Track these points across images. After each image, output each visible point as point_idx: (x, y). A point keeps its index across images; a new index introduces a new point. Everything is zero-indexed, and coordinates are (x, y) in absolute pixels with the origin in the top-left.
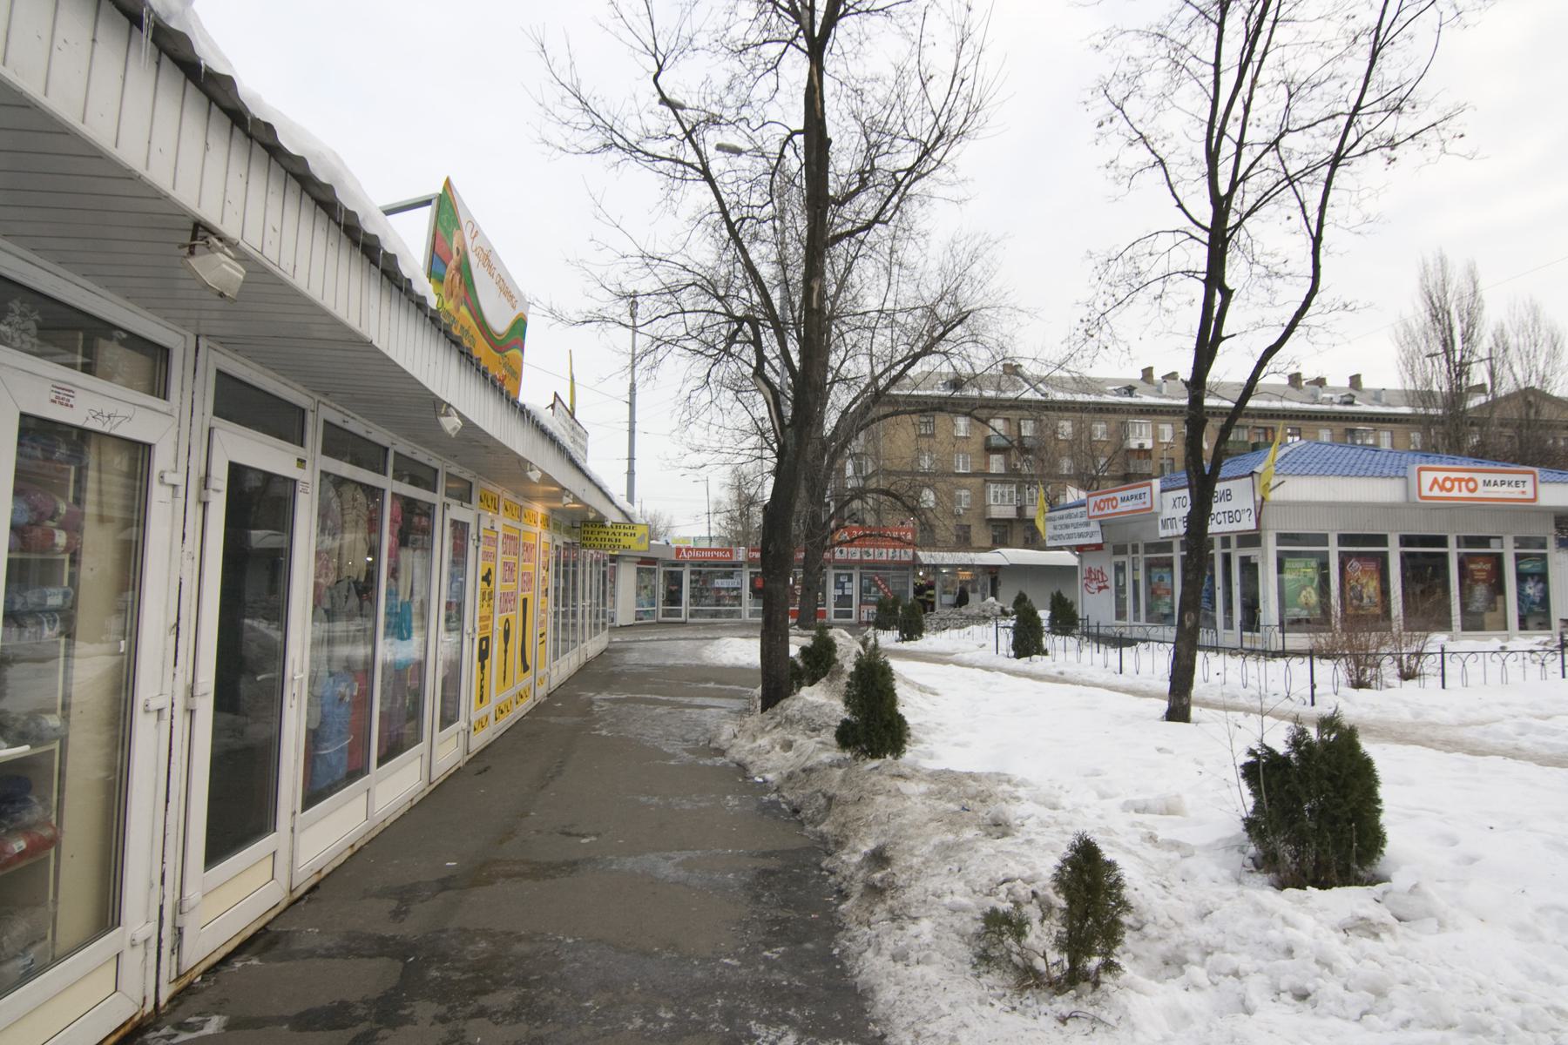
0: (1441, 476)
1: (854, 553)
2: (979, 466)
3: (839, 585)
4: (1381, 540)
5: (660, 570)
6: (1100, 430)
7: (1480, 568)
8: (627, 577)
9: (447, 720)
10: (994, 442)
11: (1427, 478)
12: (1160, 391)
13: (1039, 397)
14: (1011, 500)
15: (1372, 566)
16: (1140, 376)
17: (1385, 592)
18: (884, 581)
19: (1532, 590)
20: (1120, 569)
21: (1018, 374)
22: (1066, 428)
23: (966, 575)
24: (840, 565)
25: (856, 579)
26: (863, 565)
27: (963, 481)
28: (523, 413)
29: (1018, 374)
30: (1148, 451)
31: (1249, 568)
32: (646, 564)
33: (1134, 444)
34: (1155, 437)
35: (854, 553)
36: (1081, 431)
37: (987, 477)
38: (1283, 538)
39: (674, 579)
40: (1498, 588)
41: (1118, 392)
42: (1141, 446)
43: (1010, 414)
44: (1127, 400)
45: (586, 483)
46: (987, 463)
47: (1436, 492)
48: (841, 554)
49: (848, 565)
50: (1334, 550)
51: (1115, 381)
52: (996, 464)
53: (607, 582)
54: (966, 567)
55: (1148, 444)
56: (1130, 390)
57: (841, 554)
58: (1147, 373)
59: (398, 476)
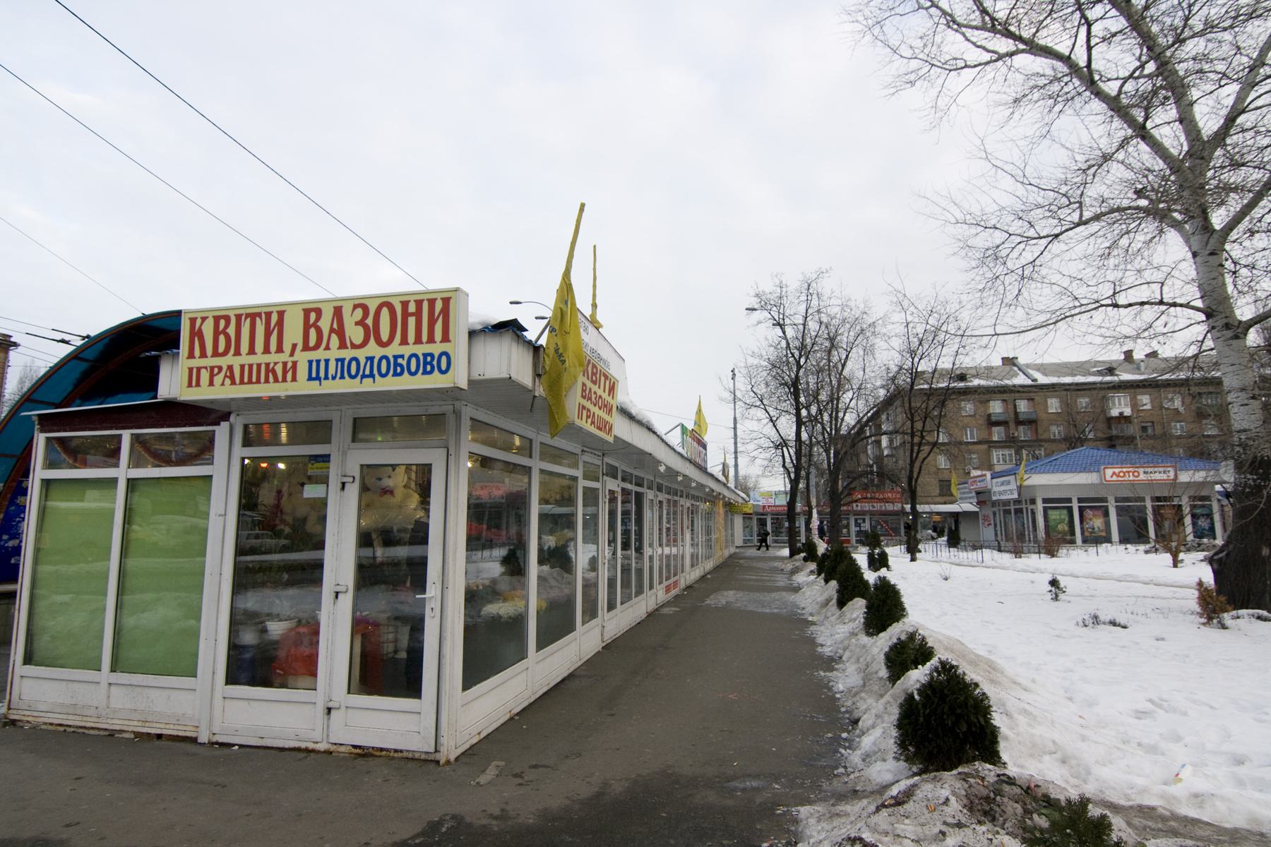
0: (1117, 471)
1: (867, 506)
2: (984, 435)
3: (857, 525)
4: (1069, 500)
5: (755, 518)
6: (1083, 401)
7: (1168, 513)
8: (738, 521)
9: (661, 583)
10: (993, 419)
11: (1109, 472)
12: (1138, 368)
13: (1029, 382)
14: (1011, 460)
15: (1100, 513)
16: (1122, 357)
17: (1108, 524)
18: (886, 522)
19: (1203, 523)
20: (994, 514)
21: (1014, 365)
22: (1054, 405)
23: (937, 518)
24: (856, 513)
25: (868, 521)
26: (872, 513)
27: (970, 447)
28: (712, 476)
29: (1014, 365)
30: (1126, 417)
31: (1033, 513)
32: (747, 517)
33: (1115, 412)
34: (1134, 406)
35: (867, 506)
36: (1068, 408)
37: (991, 445)
38: (1045, 501)
39: (762, 523)
40: (1180, 521)
41: (1100, 373)
42: (1121, 414)
43: (1005, 396)
44: (1108, 378)
45: (635, 427)
46: (990, 434)
47: (1115, 478)
48: (857, 507)
49: (863, 513)
50: (1075, 506)
51: (1097, 363)
52: (997, 434)
53: (729, 525)
54: (938, 513)
55: (1128, 412)
56: (1111, 371)
57: (857, 507)
58: (1128, 355)
59: (543, 457)
